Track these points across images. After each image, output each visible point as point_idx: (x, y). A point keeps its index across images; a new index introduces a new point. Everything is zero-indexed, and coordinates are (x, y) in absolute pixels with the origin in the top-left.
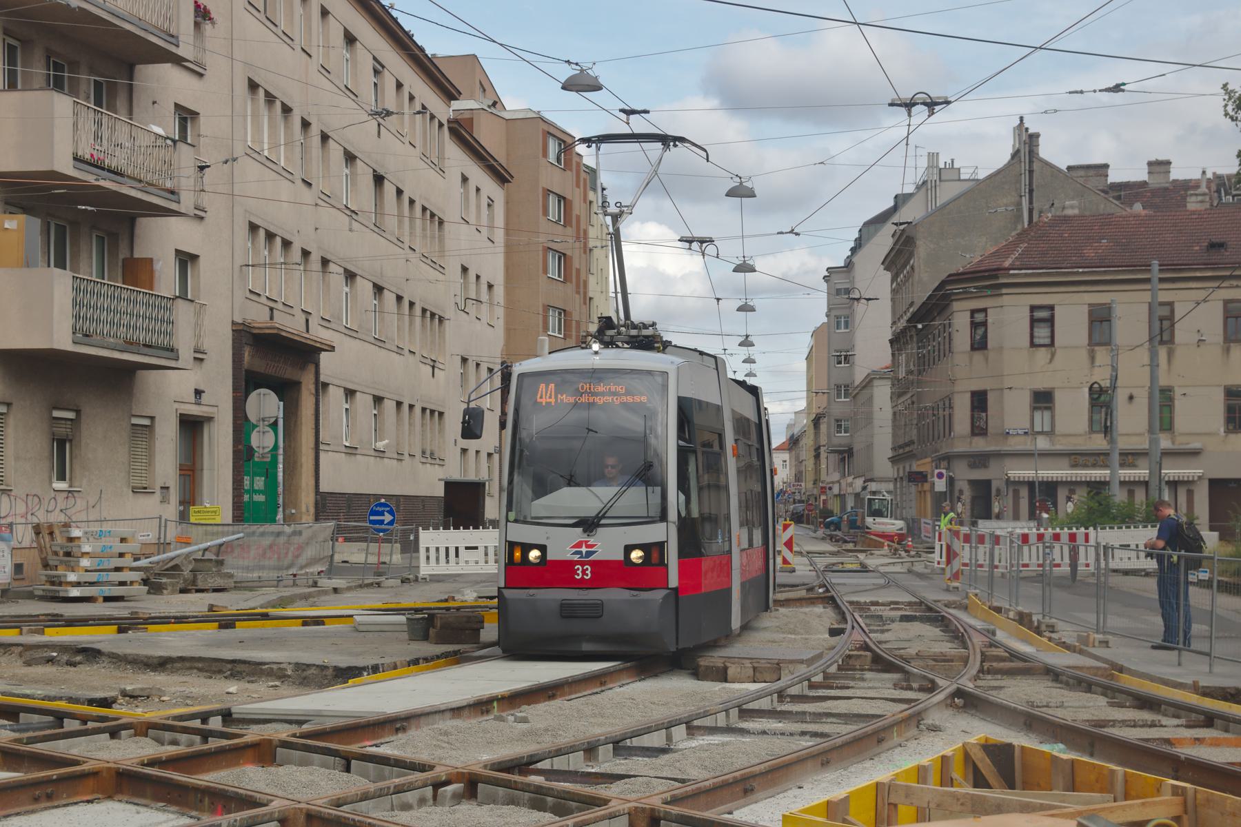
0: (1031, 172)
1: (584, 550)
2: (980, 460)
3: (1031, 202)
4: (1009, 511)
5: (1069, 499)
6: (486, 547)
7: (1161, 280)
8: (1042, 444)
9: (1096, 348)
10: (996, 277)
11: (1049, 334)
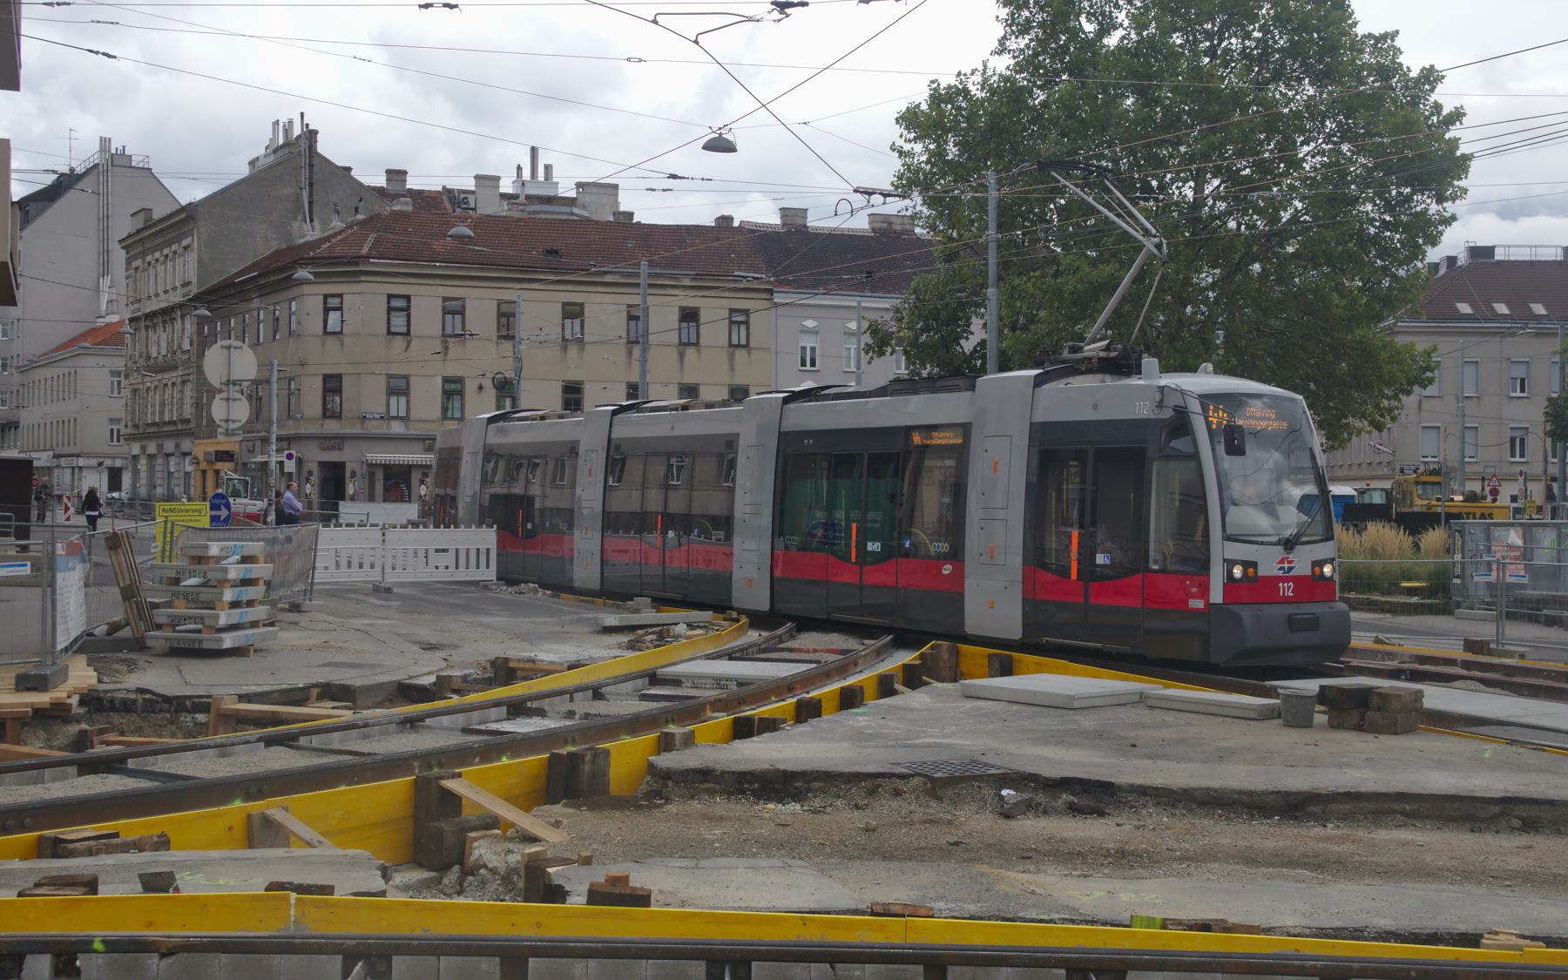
0: (311, 166)
1: (1286, 565)
2: (338, 441)
3: (311, 195)
4: (627, 500)
5: (422, 482)
6: (478, 550)
7: (651, 286)
8: (397, 428)
9: (449, 339)
10: (357, 264)
11: (405, 323)
